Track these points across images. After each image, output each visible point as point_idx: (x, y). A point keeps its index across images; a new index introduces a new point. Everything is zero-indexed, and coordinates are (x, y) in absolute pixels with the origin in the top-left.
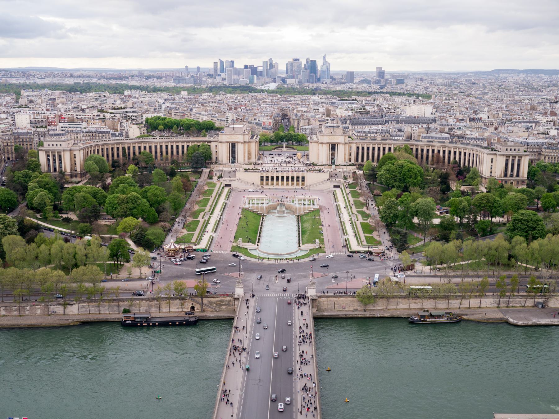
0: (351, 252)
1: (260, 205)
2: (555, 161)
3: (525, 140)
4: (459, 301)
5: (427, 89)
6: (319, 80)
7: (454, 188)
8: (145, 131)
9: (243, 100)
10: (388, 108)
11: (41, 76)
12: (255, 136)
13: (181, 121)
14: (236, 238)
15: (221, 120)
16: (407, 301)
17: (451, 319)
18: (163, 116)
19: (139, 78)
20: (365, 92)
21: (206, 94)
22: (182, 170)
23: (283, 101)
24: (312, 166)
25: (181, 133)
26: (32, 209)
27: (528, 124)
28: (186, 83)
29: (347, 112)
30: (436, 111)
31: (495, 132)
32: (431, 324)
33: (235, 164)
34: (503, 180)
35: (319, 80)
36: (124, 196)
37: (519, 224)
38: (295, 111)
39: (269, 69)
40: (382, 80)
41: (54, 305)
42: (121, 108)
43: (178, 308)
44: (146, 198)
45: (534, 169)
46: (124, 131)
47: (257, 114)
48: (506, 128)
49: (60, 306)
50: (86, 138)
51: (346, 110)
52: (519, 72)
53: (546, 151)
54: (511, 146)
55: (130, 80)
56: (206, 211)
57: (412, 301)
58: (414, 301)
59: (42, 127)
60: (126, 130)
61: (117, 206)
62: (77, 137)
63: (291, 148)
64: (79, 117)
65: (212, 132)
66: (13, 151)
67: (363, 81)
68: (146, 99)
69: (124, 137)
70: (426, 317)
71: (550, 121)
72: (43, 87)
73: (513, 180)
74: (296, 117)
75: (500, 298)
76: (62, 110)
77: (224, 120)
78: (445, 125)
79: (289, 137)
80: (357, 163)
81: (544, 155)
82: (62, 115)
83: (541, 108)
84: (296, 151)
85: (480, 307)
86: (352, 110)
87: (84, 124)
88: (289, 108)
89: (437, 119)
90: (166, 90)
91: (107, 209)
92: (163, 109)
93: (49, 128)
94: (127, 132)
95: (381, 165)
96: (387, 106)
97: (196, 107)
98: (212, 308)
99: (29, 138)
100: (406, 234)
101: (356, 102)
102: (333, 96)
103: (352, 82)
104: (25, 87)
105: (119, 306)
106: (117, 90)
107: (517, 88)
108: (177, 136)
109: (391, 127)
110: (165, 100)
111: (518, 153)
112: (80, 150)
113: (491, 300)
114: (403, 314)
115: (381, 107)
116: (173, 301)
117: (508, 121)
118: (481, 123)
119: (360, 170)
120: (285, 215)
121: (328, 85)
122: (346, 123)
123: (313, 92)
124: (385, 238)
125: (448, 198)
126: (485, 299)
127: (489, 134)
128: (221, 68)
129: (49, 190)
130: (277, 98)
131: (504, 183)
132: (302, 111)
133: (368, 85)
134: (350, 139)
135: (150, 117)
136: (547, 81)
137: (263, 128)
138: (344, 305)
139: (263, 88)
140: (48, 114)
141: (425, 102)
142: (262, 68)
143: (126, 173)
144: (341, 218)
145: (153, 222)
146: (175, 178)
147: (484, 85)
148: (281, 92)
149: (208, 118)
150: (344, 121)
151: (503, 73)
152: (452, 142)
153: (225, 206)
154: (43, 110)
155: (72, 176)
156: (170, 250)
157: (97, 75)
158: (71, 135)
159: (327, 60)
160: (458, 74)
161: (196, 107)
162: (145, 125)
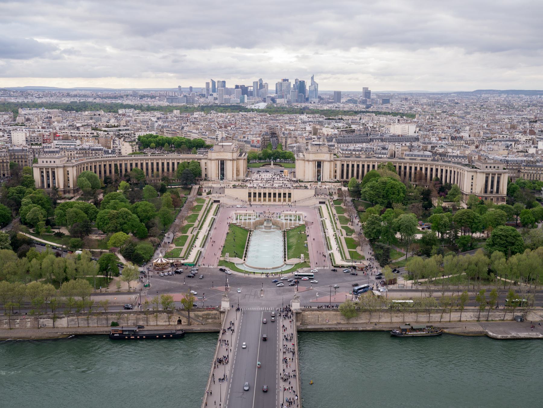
0: (335, 267)
1: (247, 221)
2: (533, 178)
3: (505, 158)
4: (439, 315)
5: (411, 108)
6: (307, 99)
7: (436, 205)
8: (137, 149)
9: (233, 119)
10: (373, 127)
11: (39, 95)
12: (244, 154)
13: (172, 139)
15: (211, 138)
16: (389, 314)
17: (432, 332)
18: (155, 134)
19: (134, 98)
20: (351, 111)
21: (198, 113)
22: (172, 187)
23: (272, 120)
24: (299, 184)
25: (172, 150)
26: (25, 224)
27: (507, 142)
28: (179, 102)
29: (333, 130)
30: (420, 130)
31: (476, 150)
32: (413, 337)
33: (224, 181)
34: (483, 196)
35: (307, 99)
36: (115, 211)
37: (499, 240)
38: (283, 129)
39: (260, 89)
40: (368, 100)
41: (44, 318)
42: (115, 126)
43: (166, 322)
44: (137, 214)
45: (514, 186)
46: (117, 149)
47: (247, 132)
48: (487, 146)
49: (49, 319)
50: (80, 155)
51: (332, 129)
52: (501, 92)
53: (524, 168)
54: (491, 163)
55: (125, 99)
56: (194, 226)
57: (394, 314)
58: (396, 314)
59: (37, 144)
60: (119, 148)
61: (108, 221)
62: (71, 155)
63: (279, 165)
64: (73, 135)
65: (202, 150)
66: (9, 168)
67: (349, 101)
68: (139, 118)
69: (117, 154)
70: (408, 330)
71: (529, 140)
72: (41, 106)
73: (493, 197)
74: (284, 135)
75: (480, 312)
76: (57, 128)
77: (214, 138)
78: (428, 143)
79: (277, 154)
80: (342, 180)
81: (523, 172)
83: (521, 127)
84: (283, 168)
85: (460, 321)
86: (338, 128)
87: (78, 142)
88: (277, 126)
89: (420, 137)
90: (159, 109)
91: (98, 224)
92: (155, 128)
93: (44, 145)
94: (120, 150)
95: (365, 182)
96: (372, 125)
97: (187, 126)
98: (199, 322)
99: (24, 155)
100: (388, 249)
101: (342, 121)
102: (321, 115)
103: (340, 102)
104: (23, 105)
105: (107, 319)
106: (112, 109)
107: (499, 108)
108: (168, 153)
109: (376, 145)
110: (158, 119)
111: (497, 171)
112: (73, 167)
113: (472, 314)
114: (386, 328)
115: (366, 125)
116: (160, 315)
117: (489, 139)
118: (462, 142)
119: (345, 186)
120: (272, 230)
121: (316, 105)
122: (332, 141)
123: (301, 111)
125: (430, 214)
126: (465, 313)
127: (470, 152)
128: (213, 88)
129: (42, 206)
130: (266, 117)
131: (484, 199)
132: (290, 130)
133: (355, 105)
134: (335, 156)
135: (143, 135)
136: (527, 101)
137: (252, 146)
138: (328, 318)
139: (253, 107)
140: (43, 132)
141: (409, 121)
142: (252, 88)
144: (326, 234)
145: (143, 237)
146: (165, 194)
147: (466, 105)
148: (271, 111)
149: (199, 136)
150: (330, 139)
151: (485, 94)
152: (434, 160)
153: (213, 221)
154: (38, 128)
155: (65, 192)
156: (157, 265)
157: (92, 95)
158: (65, 152)
159: (315, 80)
160: (442, 94)
161: (187, 126)
162: (137, 143)
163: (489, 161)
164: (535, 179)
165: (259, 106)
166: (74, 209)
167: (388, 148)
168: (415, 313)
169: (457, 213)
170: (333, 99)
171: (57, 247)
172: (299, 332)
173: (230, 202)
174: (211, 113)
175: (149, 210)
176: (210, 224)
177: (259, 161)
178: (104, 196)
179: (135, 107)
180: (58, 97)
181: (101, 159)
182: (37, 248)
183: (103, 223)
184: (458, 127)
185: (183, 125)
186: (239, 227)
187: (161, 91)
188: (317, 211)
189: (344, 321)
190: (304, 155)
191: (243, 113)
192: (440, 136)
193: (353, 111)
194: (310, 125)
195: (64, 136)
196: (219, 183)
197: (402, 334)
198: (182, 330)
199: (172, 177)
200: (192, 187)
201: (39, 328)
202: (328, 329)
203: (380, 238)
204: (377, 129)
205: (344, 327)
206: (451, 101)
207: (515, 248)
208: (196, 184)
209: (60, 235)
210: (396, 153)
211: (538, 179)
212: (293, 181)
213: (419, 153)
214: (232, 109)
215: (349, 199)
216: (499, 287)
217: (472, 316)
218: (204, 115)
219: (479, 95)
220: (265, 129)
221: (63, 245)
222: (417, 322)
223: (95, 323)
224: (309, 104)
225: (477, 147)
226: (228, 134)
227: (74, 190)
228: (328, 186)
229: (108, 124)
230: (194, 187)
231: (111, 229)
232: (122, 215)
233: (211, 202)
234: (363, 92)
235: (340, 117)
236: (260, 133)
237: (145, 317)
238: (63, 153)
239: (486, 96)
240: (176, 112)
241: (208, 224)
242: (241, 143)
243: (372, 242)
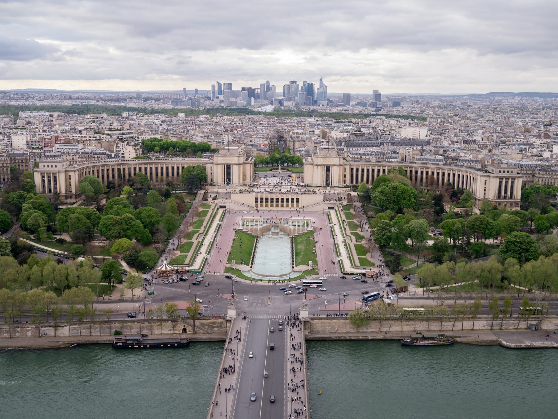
0: (344, 274)
1: (254, 227)
2: (548, 183)
3: (519, 162)
4: (452, 323)
5: (422, 111)
6: (316, 102)
7: (448, 210)
8: (141, 153)
9: (239, 122)
10: (383, 130)
11: (40, 98)
12: (251, 158)
13: (177, 142)
14: (229, 260)
15: (217, 142)
16: (400, 323)
17: (444, 341)
18: (159, 138)
19: (138, 100)
20: (361, 114)
21: (203, 116)
22: (177, 192)
23: (280, 123)
24: (308, 188)
25: (176, 154)
26: (26, 230)
27: (521, 146)
28: (184, 105)
29: (342, 134)
30: (431, 134)
31: (489, 154)
32: (424, 346)
33: (230, 185)
34: (497, 202)
35: (316, 102)
36: (118, 217)
37: (512, 246)
38: (291, 133)
39: (267, 91)
40: (378, 103)
41: (45, 327)
42: (118, 130)
43: (170, 330)
44: (140, 219)
45: (528, 191)
46: (120, 153)
47: (253, 136)
48: (500, 150)
49: (51, 328)
50: (82, 159)
51: (341, 132)
52: (514, 95)
53: (539, 173)
54: (504, 168)
55: (128, 102)
56: (200, 232)
57: (404, 323)
58: (407, 323)
59: (38, 148)
60: (122, 152)
61: (111, 227)
62: (73, 159)
63: (286, 169)
64: (75, 138)
65: (208, 154)
66: (9, 172)
67: (359, 104)
68: (143, 121)
70: (419, 339)
71: (544, 144)
72: (42, 108)
73: (507, 202)
74: (292, 139)
75: (493, 320)
76: (59, 132)
77: (220, 142)
78: (440, 147)
79: (284, 158)
80: (351, 185)
81: (537, 177)
82: (59, 137)
83: (535, 130)
84: (291, 172)
85: (473, 330)
86: (347, 132)
87: (80, 146)
88: (285, 130)
89: (431, 141)
90: (163, 111)
91: (101, 230)
92: (160, 131)
93: (46, 149)
94: (123, 154)
95: (375, 187)
96: (382, 129)
97: (193, 129)
98: (204, 330)
99: (25, 160)
100: (399, 255)
101: (351, 124)
102: (330, 118)
103: (349, 105)
104: (24, 108)
105: (110, 328)
106: (115, 112)
107: (512, 111)
108: (173, 158)
109: (386, 149)
110: (162, 122)
111: (511, 175)
112: (75, 171)
113: (485, 322)
114: (396, 337)
116: (165, 323)
118: (475, 146)
119: (354, 191)
120: (279, 236)
121: (325, 107)
122: (341, 145)
123: (309, 114)
124: (376, 258)
125: (442, 220)
126: (478, 321)
127: (483, 156)
128: (219, 90)
129: (43, 211)
130: (273, 120)
131: (497, 205)
132: (298, 133)
133: (365, 108)
134: (344, 161)
135: (147, 139)
136: (541, 104)
137: (259, 150)
138: (337, 327)
139: (260, 110)
140: (44, 136)
141: (420, 125)
142: (259, 90)
143: (121, 195)
144: (335, 240)
145: (147, 244)
146: (169, 200)
147: (479, 108)
148: (278, 114)
149: (204, 140)
150: (339, 143)
151: (498, 96)
152: (446, 164)
153: (219, 227)
154: (40, 131)
155: (67, 197)
156: (161, 272)
157: (95, 97)
158: (66, 156)
159: (324, 83)
160: (454, 96)
161: (193, 129)
163: (502, 166)
164: (550, 184)
165: (266, 109)
166: (77, 215)
167: (398, 152)
168: (426, 321)
169: (470, 218)
170: (342, 102)
171: (59, 254)
172: (308, 341)
173: (236, 208)
174: (217, 116)
175: (153, 216)
176: (215, 230)
177: (266, 165)
178: (106, 202)
179: (138, 110)
181: (103, 164)
182: (38, 254)
183: (106, 229)
184: (471, 131)
185: (188, 128)
186: (246, 233)
187: (166, 93)
188: (326, 216)
189: (354, 329)
190: (312, 160)
191: (250, 116)
192: (452, 140)
193: (363, 114)
194: (318, 128)
195: (66, 140)
196: (225, 188)
197: (413, 343)
198: (187, 339)
199: (177, 181)
200: (197, 192)
201: (40, 337)
202: (337, 338)
203: (391, 244)
204: (388, 133)
205: (353, 336)
206: (464, 104)
207: (530, 255)
208: (201, 189)
209: (61, 241)
210: (407, 157)
211: (553, 184)
212: (301, 186)
213: (430, 157)
214: (238, 112)
215: (359, 204)
216: (512, 295)
217: (485, 324)
218: (210, 118)
219: (492, 98)
220: (273, 132)
221: (65, 252)
222: (428, 331)
223: (97, 332)
224: (318, 107)
225: (490, 151)
226: (235, 138)
227: (76, 195)
228: (337, 191)
229: (111, 127)
230: (199, 192)
231: (114, 235)
233: (216, 208)
234: (373, 95)
235: (350, 121)
236: (267, 136)
237: (149, 326)
238: (64, 157)
239: (500, 98)
240: (181, 115)
242: (247, 147)
243: (382, 248)
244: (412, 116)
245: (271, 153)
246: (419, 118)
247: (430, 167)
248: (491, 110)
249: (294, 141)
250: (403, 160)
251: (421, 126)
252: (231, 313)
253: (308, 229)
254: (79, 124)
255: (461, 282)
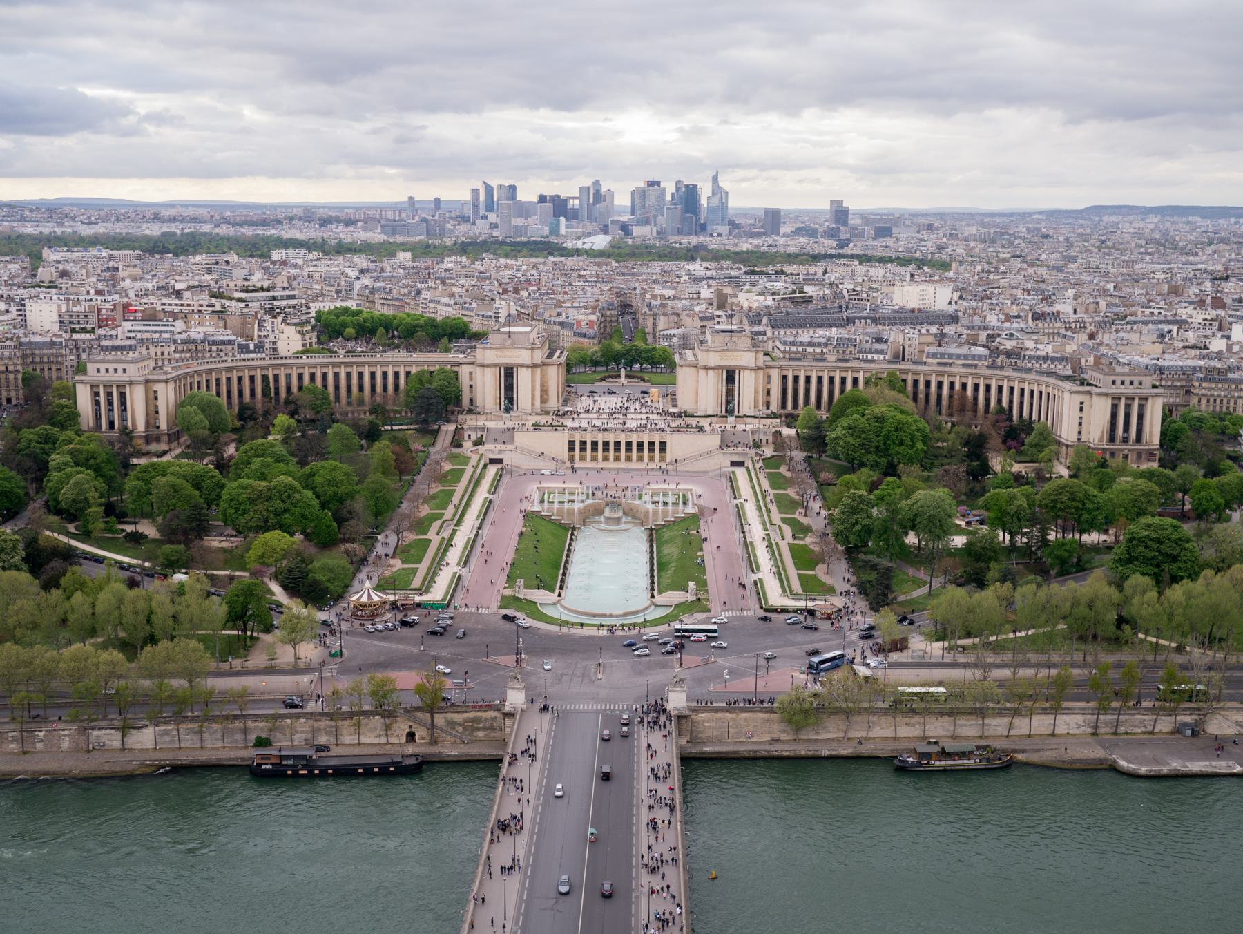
0: (766, 610)
1: (566, 506)
2: (1221, 407)
3: (1155, 362)
5: (941, 248)
6: (703, 228)
7: (998, 468)
8: (314, 340)
9: (533, 272)
10: (854, 291)
11: (89, 218)
12: (558, 352)
13: (395, 317)
15: (483, 316)
16: (890, 719)
17: (988, 760)
18: (354, 308)
19: (306, 224)
20: (804, 254)
21: (453, 258)
22: (394, 428)
23: (623, 274)
24: (685, 420)
25: (393, 344)
26: (58, 512)
27: (1162, 326)
28: (409, 235)
29: (762, 298)
30: (961, 298)
31: (1090, 343)
32: (946, 771)
33: (512, 413)
34: (1107, 449)
35: (703, 228)
36: (264, 484)
37: (1141, 549)
38: (648, 296)
39: (594, 204)
40: (843, 229)
41: (101, 729)
42: (262, 289)
43: (379, 736)
44: (313, 489)
45: (1176, 426)
46: (267, 340)
47: (564, 302)
48: (1114, 335)
49: (113, 731)
50: (183, 355)
51: (760, 294)
52: (1146, 211)
53: (1201, 385)
54: (1123, 374)
55: (286, 227)
56: (445, 518)
57: (901, 720)
58: (907, 720)
59: (84, 330)
60: (272, 338)
61: (248, 506)
62: (162, 354)
63: (638, 377)
64: (167, 308)
65: (463, 343)
66: (20, 384)
67: (799, 232)
68: (319, 269)
70: (934, 756)
71: (1212, 320)
72: (93, 242)
73: (1129, 450)
74: (650, 310)
75: (1099, 714)
76: (132, 294)
77: (491, 317)
78: (980, 328)
79: (633, 353)
80: (782, 412)
81: (1197, 395)
82: (131, 305)
83: (1192, 291)
84: (648, 384)
85: (1053, 735)
86: (774, 294)
87: (179, 325)
88: (635, 289)
89: (960, 314)
90: (364, 249)
91: (224, 513)
92: (356, 292)
93: (102, 332)
94: (274, 343)
95: (836, 417)
96: (851, 287)
97: (429, 288)
98: (455, 736)
99: (56, 356)
100: (889, 569)
101: (783, 276)
102: (734, 263)
103: (778, 233)
104: (53, 241)
105: (245, 731)
106: (257, 249)
107: (1142, 246)
108: (385, 351)
109: (860, 332)
110: (362, 271)
111: (1138, 391)
112: (167, 382)
113: (1079, 719)
114: (883, 750)
116: (367, 720)
117: (1119, 319)
118: (1058, 325)
119: (789, 426)
120: (622, 526)
121: (723, 239)
122: (759, 323)
123: (689, 254)
125: (984, 491)
126: (1065, 716)
127: (1075, 348)
128: (488, 200)
129: (95, 471)
130: (609, 268)
132: (663, 297)
133: (812, 240)
134: (767, 358)
135: (326, 309)
136: (1206, 232)
137: (576, 334)
138: (751, 728)
139: (579, 245)
140: (99, 302)
141: (937, 278)
142: (577, 202)
143: (270, 434)
144: (747, 535)
145: (327, 543)
146: (377, 445)
148: (619, 255)
149: (455, 312)
150: (755, 318)
151: (1110, 214)
152: (993, 366)
153: (489, 507)
154: (88, 292)
155: (148, 439)
156: (359, 607)
157: (212, 216)
158: (148, 348)
159: (721, 184)
160: (1012, 215)
161: (429, 288)
163: (1119, 370)
164: (1224, 409)
165: (593, 244)
166: (170, 478)
167: (887, 339)
168: (950, 716)
169: (1047, 487)
170: (763, 227)
171: (130, 566)
172: (685, 760)
174: (483, 259)
175: (341, 482)
176: (480, 513)
177: (594, 369)
178: (237, 449)
179: (308, 245)
180: (132, 221)
181: (230, 365)
182: (84, 567)
183: (237, 510)
184: (1048, 291)
185: (419, 285)
187: (369, 208)
188: (725, 482)
189: (788, 734)
190: (695, 356)
191: (557, 259)
192: (1006, 311)
193: (808, 254)
194: (709, 286)
195: (147, 312)
196: (501, 418)
197: (920, 764)
198: (416, 756)
199: (394, 404)
200: (439, 428)
201: (89, 751)
202: (752, 754)
203: (870, 544)
204: (864, 296)
205: (786, 750)
206: (1033, 232)
207: (1180, 568)
208: (448, 422)
209: (136, 538)
210: (907, 349)
211: (1231, 409)
212: (670, 414)
213: (959, 351)
214: (531, 250)
215: (799, 455)
216: (1141, 657)
217: (1081, 723)
218: (467, 264)
219: (1097, 219)
220: (608, 295)
221: (144, 561)
222: (954, 737)
223: (217, 740)
224: (708, 239)
225: (1092, 337)
226: (522, 307)
227: (169, 435)
228: (751, 425)
229: (247, 283)
230: (444, 428)
231: (254, 525)
232: (279, 492)
233: (482, 463)
234: (831, 212)
235: (779, 269)
236: (595, 303)
237: (332, 727)
238: (144, 350)
239: (1113, 219)
241: (476, 513)
242: (551, 327)
243: (851, 553)
244: (917, 259)
245: (603, 341)
246: (933, 264)
247: (958, 373)
248: (1093, 245)
249: (655, 315)
250: (898, 358)
251: (937, 282)
252: (516, 698)
253: (686, 511)
254: (176, 277)
255: (1028, 629)
